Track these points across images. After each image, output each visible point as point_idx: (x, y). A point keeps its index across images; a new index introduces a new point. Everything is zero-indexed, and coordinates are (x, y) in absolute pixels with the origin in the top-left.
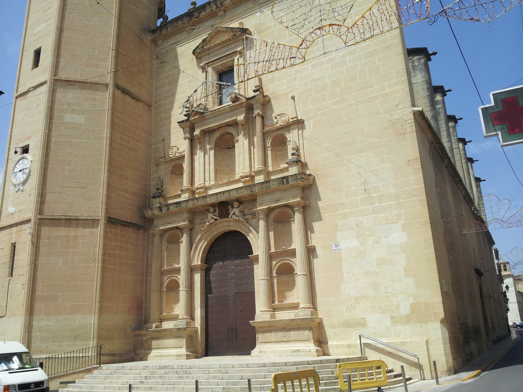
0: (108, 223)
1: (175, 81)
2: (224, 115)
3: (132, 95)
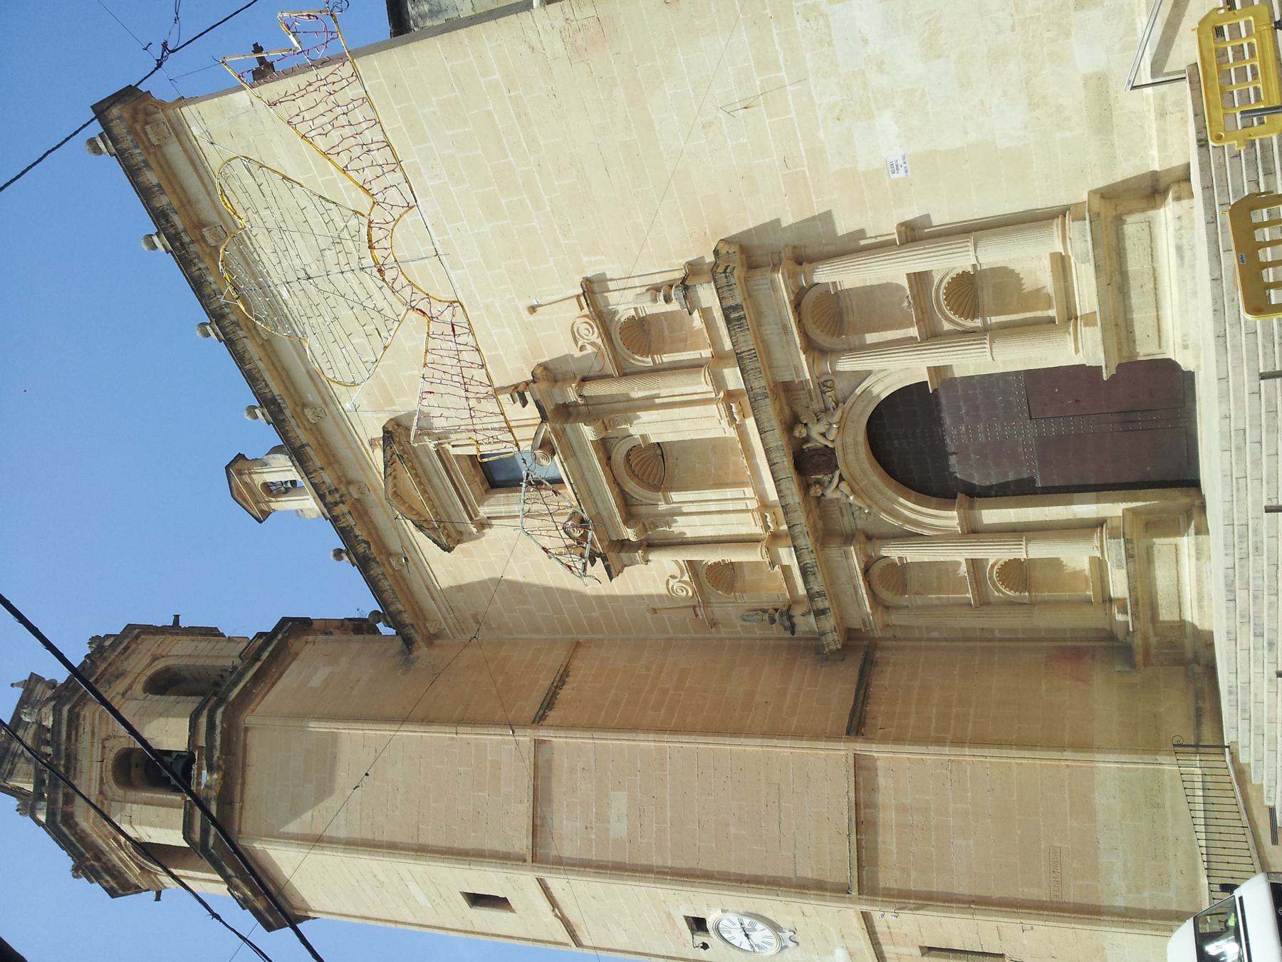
0: (863, 735)
1: (517, 589)
3: (555, 685)
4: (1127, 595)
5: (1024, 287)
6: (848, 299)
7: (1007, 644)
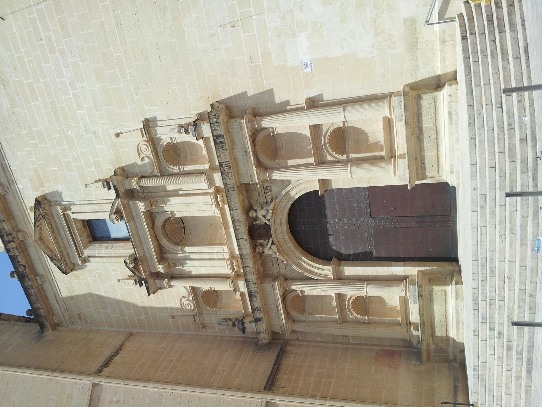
0: (272, 390)
1: (101, 301)
2: (139, 230)
3: (112, 354)
4: (419, 322)
5: (369, 138)
6: (280, 142)
7: (355, 346)
